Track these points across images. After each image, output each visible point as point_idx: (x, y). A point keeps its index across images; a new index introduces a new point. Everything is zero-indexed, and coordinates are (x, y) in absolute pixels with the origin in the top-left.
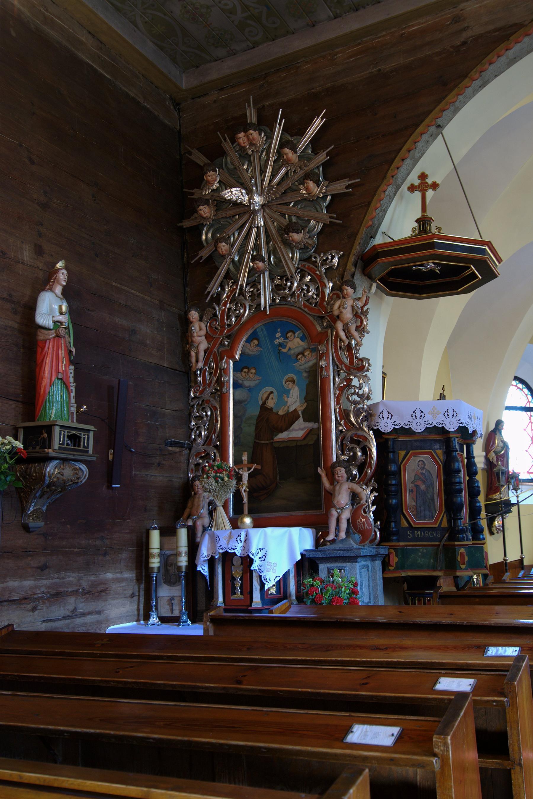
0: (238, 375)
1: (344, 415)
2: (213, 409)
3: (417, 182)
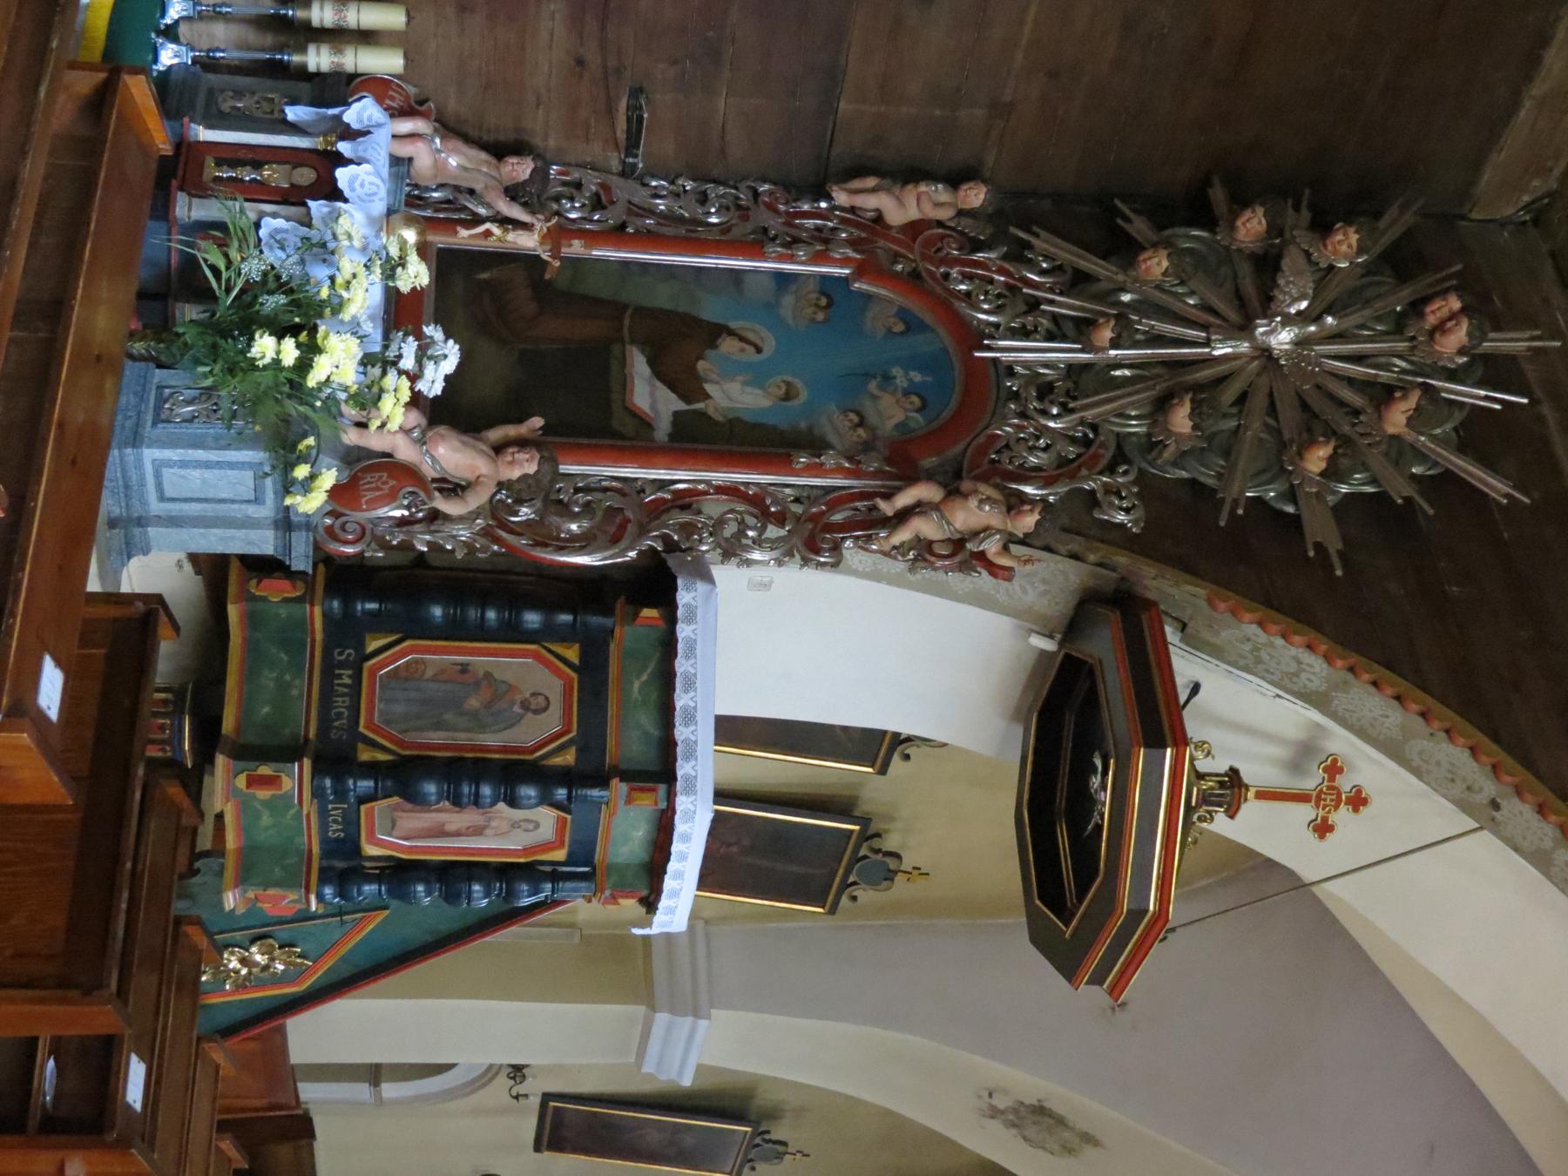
0: (811, 285)
1: (685, 501)
2: (724, 228)
3: (1345, 783)
